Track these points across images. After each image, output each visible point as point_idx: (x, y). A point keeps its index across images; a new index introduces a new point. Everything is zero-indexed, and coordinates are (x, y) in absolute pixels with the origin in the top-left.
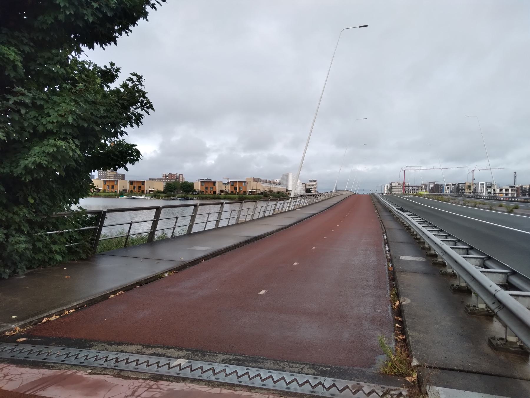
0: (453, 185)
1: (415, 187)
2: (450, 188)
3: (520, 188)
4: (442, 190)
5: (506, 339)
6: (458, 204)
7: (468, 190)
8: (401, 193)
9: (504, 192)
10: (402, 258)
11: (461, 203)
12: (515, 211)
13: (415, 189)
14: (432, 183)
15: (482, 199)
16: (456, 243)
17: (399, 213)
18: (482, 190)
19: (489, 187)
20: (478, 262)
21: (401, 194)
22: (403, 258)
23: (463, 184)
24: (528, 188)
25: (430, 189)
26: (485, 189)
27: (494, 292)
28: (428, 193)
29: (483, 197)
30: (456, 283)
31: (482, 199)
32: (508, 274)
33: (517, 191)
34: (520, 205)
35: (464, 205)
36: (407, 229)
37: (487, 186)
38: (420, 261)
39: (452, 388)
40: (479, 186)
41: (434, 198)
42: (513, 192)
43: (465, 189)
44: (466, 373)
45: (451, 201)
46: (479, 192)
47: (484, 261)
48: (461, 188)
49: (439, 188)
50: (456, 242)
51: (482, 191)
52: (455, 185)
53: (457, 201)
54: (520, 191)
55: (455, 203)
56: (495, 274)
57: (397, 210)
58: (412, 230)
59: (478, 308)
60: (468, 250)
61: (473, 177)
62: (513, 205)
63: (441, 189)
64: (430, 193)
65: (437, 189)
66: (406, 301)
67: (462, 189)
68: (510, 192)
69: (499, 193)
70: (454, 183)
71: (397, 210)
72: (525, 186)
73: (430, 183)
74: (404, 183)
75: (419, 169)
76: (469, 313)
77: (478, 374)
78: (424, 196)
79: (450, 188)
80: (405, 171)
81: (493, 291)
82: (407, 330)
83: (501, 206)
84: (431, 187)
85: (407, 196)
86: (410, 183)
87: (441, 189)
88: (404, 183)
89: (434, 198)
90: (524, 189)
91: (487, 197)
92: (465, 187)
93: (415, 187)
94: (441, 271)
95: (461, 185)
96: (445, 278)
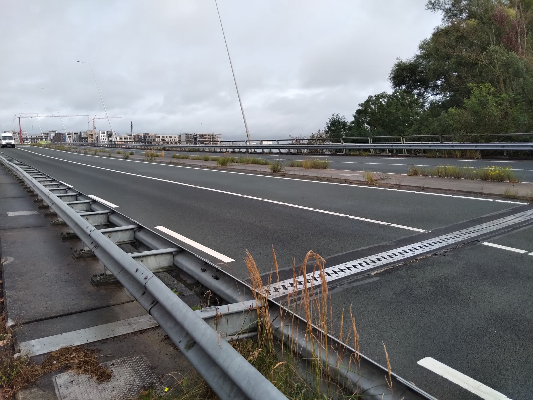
0: (75, 133)
1: (34, 137)
2: (73, 137)
3: (137, 137)
4: (64, 139)
5: (105, 274)
6: (79, 153)
7: (91, 138)
8: (19, 143)
9: (123, 139)
10: (10, 214)
11: (83, 151)
12: (131, 157)
13: (34, 139)
14: (53, 132)
15: (104, 147)
16: (66, 191)
17: (10, 165)
18: (103, 138)
19: (110, 135)
20: (84, 207)
21: (18, 144)
22: (12, 214)
23: (85, 133)
24: (143, 137)
25: (52, 138)
26: (106, 137)
27: (89, 232)
28: (49, 142)
29: (105, 146)
30: (65, 231)
31: (104, 147)
32: (108, 214)
33: (134, 139)
34: (135, 151)
35: (85, 153)
36: (20, 182)
37: (108, 135)
38: (33, 215)
39: (48, 336)
40: (101, 134)
41: (54, 147)
42: (131, 140)
43: (87, 138)
44: (65, 316)
45: (72, 150)
46: (101, 140)
47: (90, 205)
48: (83, 137)
49: (60, 137)
50: (67, 190)
51: (104, 139)
52: (77, 133)
53: (78, 150)
54: (137, 139)
55: (76, 152)
56: (97, 216)
57: (8, 162)
58: (25, 183)
59: (84, 251)
60: (77, 197)
61: (94, 125)
62: (128, 151)
63: (63, 138)
64: (52, 142)
65: (59, 137)
66: (8, 260)
67: (85, 138)
68: (129, 140)
69: (120, 142)
70: (76, 132)
71: (8, 162)
72: (141, 135)
73: (50, 132)
74: (21, 132)
75: (35, 117)
76: (77, 258)
77: (77, 313)
78: (43, 146)
79: (73, 137)
80: (20, 118)
81: (88, 231)
82: (5, 291)
83: (119, 153)
84: (52, 136)
85: (24, 147)
86: (27, 131)
87: (63, 138)
88: (21, 132)
89: (54, 147)
90: (140, 137)
91: (110, 145)
92: (87, 136)
93: (34, 137)
94: (52, 222)
95: (83, 134)
96: (57, 228)
